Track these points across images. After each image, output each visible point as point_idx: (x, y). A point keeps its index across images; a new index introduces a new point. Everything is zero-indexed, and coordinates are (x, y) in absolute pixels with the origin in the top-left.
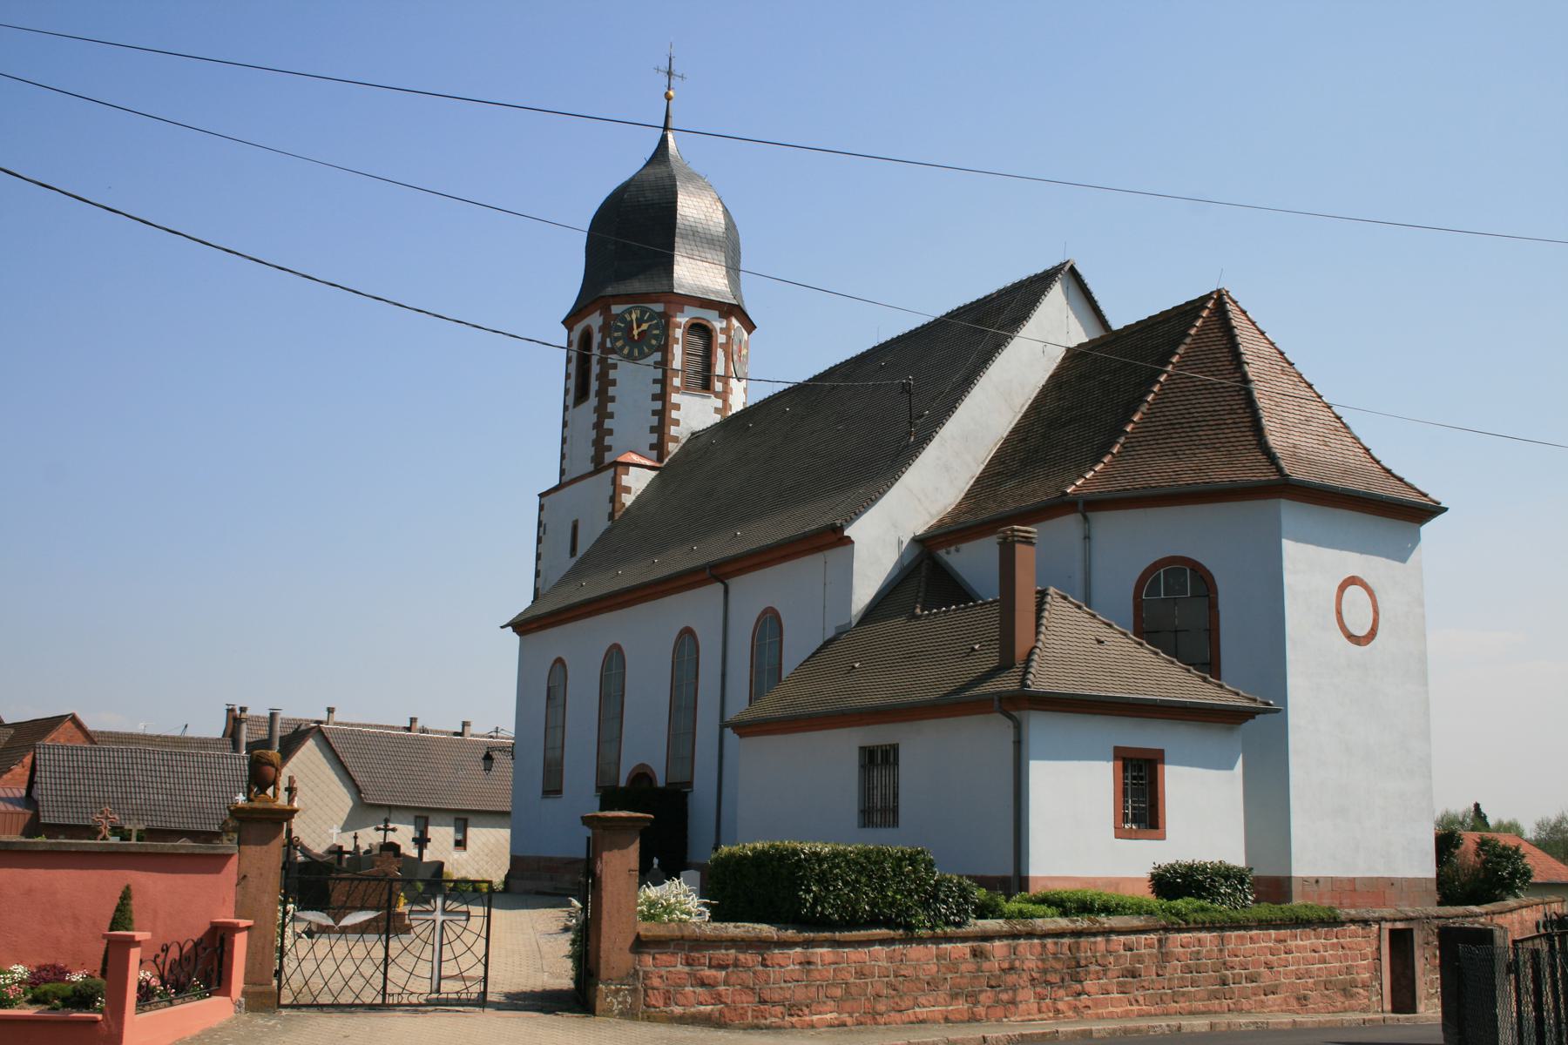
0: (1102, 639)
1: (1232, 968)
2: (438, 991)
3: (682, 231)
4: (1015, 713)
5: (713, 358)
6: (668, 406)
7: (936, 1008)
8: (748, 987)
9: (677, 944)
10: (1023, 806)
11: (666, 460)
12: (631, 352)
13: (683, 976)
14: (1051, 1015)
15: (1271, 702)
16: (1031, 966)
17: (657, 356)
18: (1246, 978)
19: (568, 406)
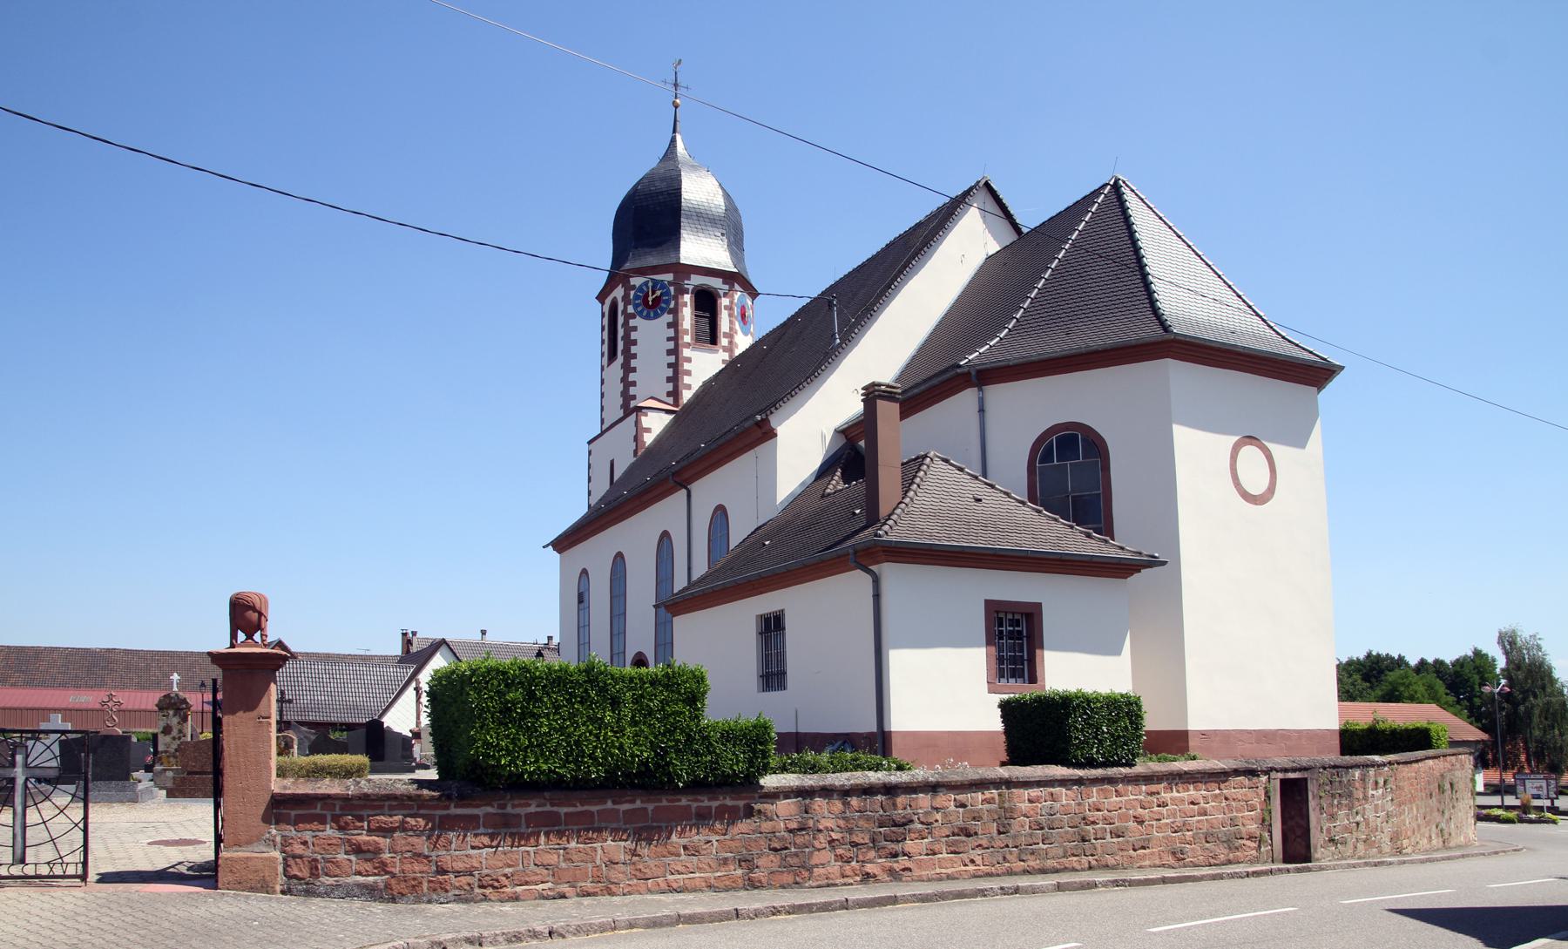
0: (979, 497)
1: (1094, 823)
2: (23, 861)
3: (687, 213)
4: (873, 568)
7: (697, 875)
8: (419, 855)
9: (325, 803)
12: (648, 314)
13: (334, 841)
14: (858, 878)
15: (1157, 555)
16: (829, 825)
17: (668, 318)
18: (1111, 833)
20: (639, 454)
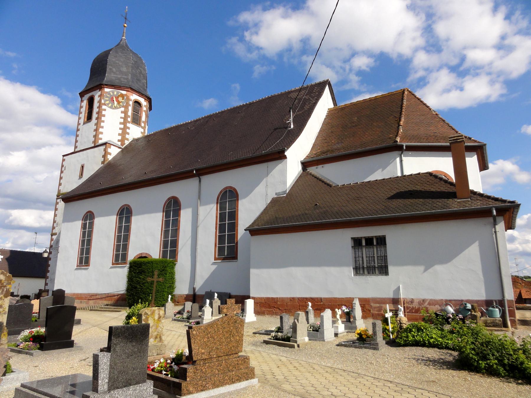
10: (427, 153)
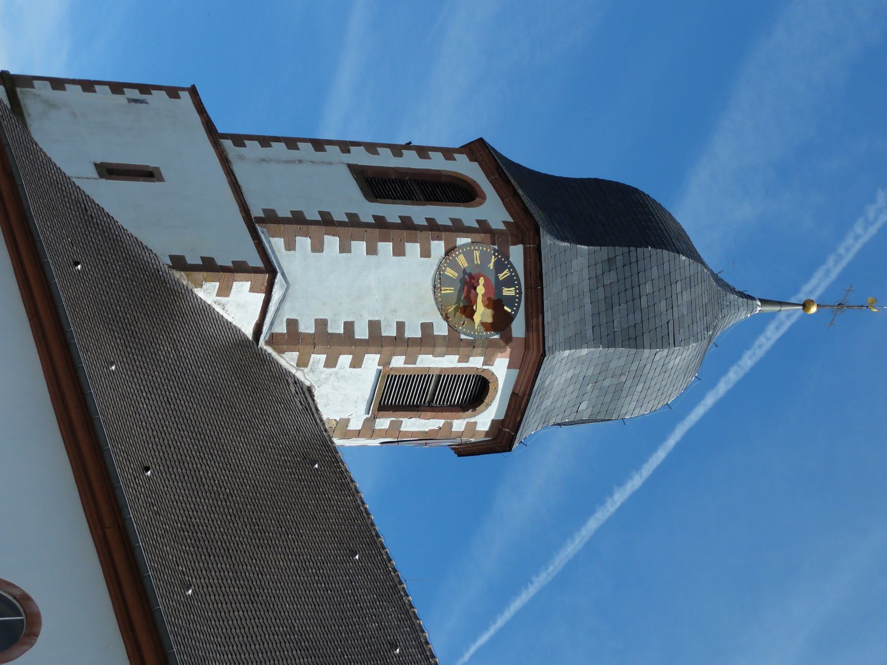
5: (429, 414)
6: (359, 349)
11: (269, 350)
12: (449, 281)
17: (441, 329)
19: (400, 155)
20: (177, 274)
